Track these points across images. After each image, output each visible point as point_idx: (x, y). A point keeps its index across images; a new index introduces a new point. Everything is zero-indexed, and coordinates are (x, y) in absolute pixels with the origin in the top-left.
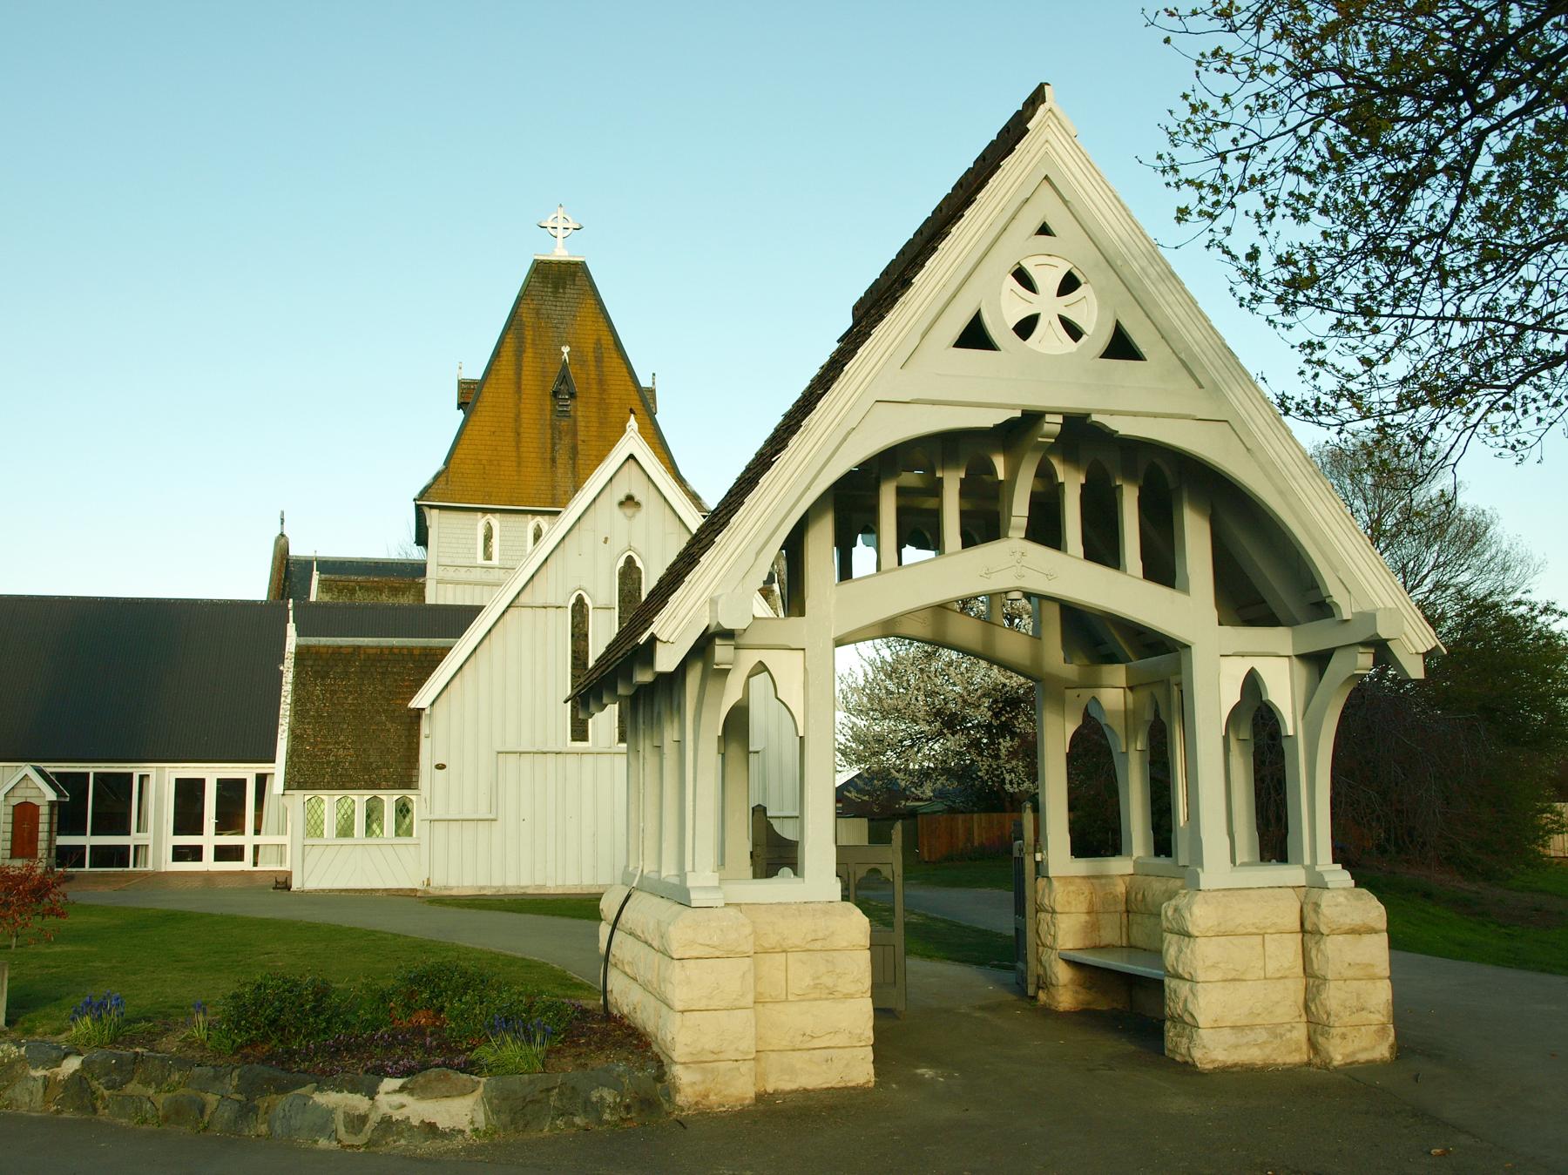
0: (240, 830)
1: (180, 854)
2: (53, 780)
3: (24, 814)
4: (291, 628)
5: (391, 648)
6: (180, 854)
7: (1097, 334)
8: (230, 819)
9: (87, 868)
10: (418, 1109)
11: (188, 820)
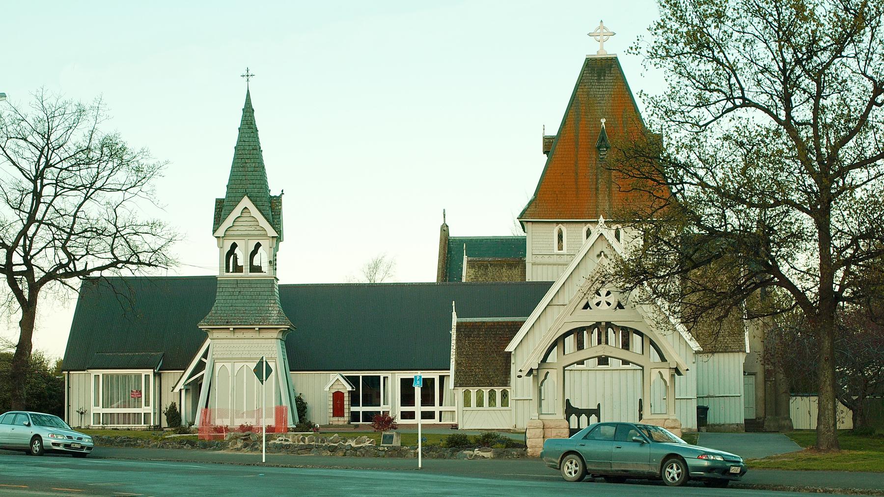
0: (433, 404)
1: (404, 415)
2: (353, 381)
3: (338, 397)
4: (454, 314)
5: (498, 322)
6: (404, 415)
7: (614, 304)
8: (428, 399)
9: (361, 422)
10: (481, 454)
11: (407, 398)
